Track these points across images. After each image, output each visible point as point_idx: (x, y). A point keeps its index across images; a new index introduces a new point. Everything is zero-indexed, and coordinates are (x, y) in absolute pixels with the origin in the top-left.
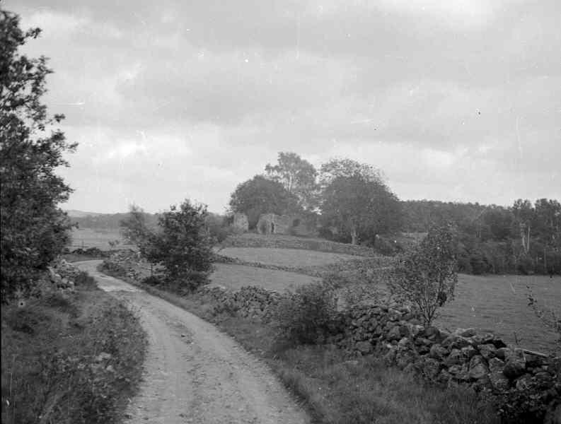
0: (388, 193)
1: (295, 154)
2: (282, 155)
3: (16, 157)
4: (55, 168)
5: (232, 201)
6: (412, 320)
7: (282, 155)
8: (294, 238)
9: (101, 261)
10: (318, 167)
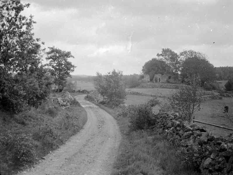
0: (210, 64)
1: (169, 49)
2: (163, 50)
3: (59, 56)
4: (68, 58)
5: (143, 69)
6: (179, 120)
7: (163, 50)
8: (169, 84)
9: (86, 95)
10: (178, 54)
